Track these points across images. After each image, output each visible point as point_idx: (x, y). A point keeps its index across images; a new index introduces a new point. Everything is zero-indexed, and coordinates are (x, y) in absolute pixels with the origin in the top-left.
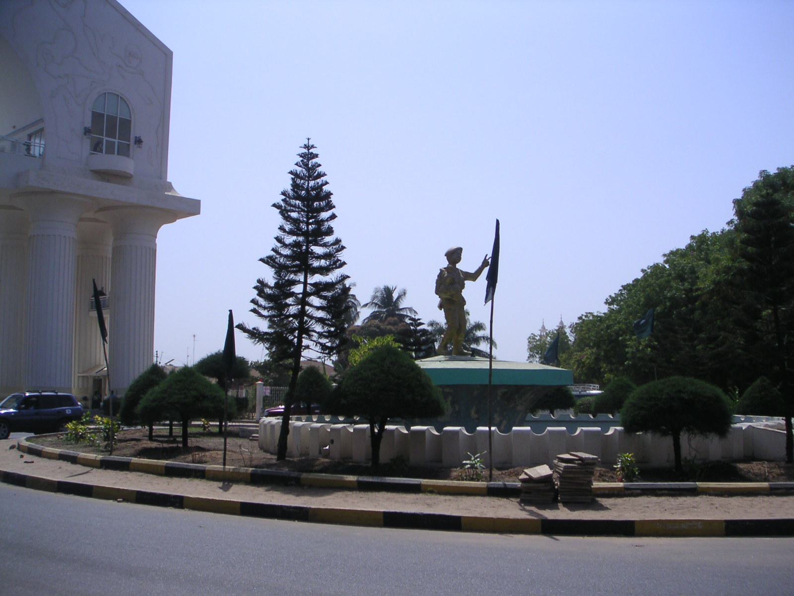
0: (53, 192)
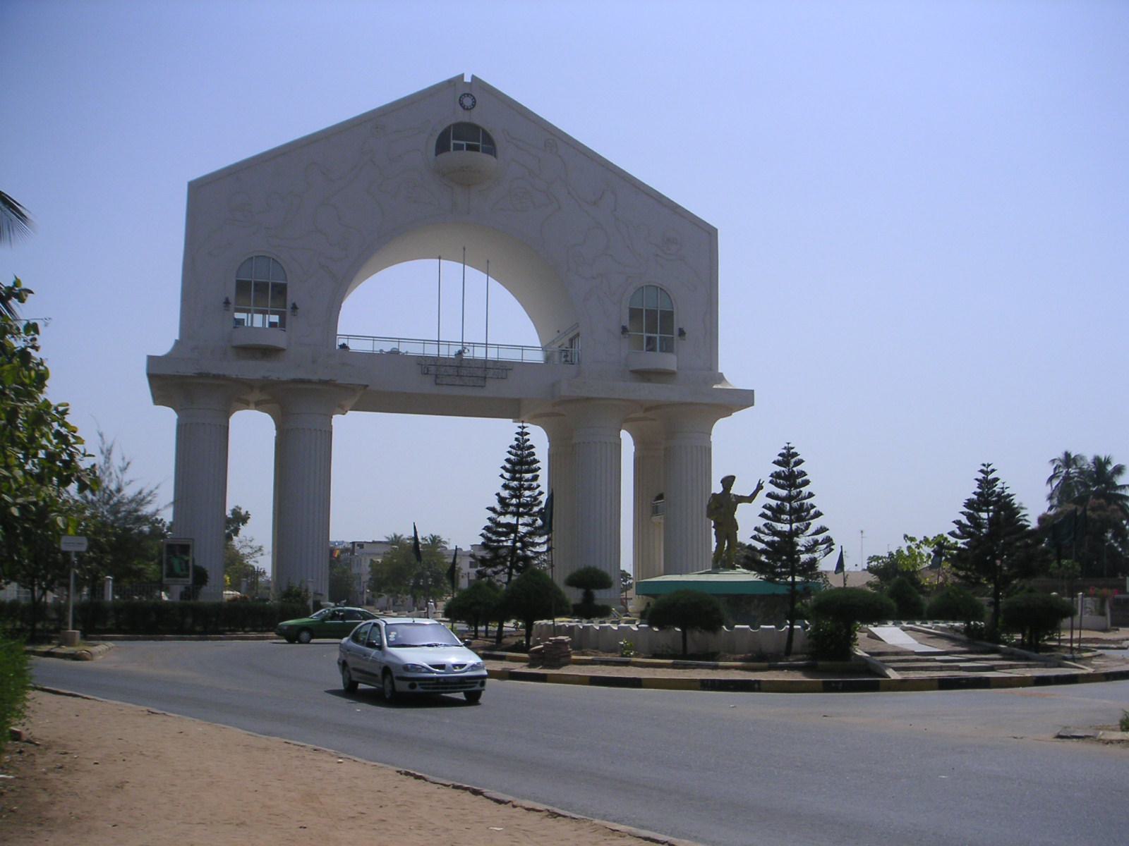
0: (588, 399)
